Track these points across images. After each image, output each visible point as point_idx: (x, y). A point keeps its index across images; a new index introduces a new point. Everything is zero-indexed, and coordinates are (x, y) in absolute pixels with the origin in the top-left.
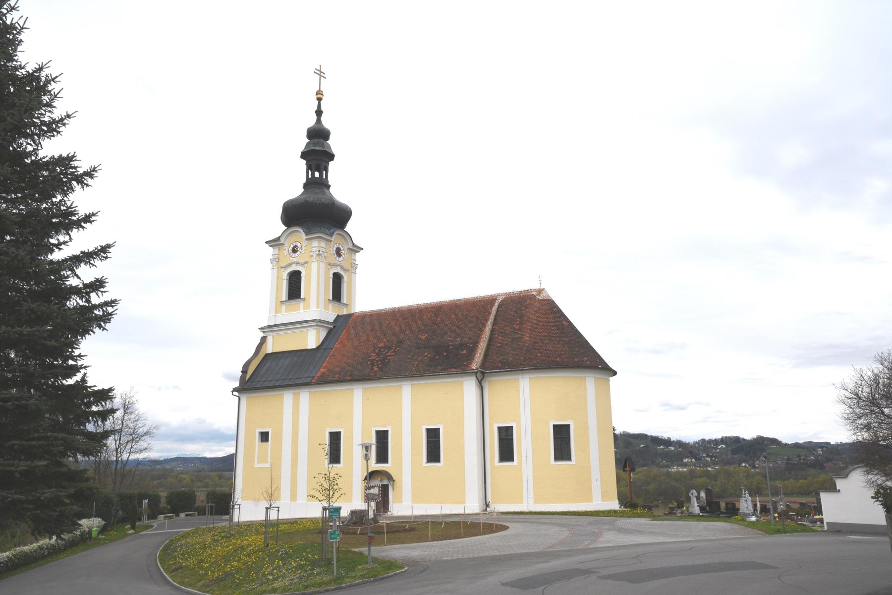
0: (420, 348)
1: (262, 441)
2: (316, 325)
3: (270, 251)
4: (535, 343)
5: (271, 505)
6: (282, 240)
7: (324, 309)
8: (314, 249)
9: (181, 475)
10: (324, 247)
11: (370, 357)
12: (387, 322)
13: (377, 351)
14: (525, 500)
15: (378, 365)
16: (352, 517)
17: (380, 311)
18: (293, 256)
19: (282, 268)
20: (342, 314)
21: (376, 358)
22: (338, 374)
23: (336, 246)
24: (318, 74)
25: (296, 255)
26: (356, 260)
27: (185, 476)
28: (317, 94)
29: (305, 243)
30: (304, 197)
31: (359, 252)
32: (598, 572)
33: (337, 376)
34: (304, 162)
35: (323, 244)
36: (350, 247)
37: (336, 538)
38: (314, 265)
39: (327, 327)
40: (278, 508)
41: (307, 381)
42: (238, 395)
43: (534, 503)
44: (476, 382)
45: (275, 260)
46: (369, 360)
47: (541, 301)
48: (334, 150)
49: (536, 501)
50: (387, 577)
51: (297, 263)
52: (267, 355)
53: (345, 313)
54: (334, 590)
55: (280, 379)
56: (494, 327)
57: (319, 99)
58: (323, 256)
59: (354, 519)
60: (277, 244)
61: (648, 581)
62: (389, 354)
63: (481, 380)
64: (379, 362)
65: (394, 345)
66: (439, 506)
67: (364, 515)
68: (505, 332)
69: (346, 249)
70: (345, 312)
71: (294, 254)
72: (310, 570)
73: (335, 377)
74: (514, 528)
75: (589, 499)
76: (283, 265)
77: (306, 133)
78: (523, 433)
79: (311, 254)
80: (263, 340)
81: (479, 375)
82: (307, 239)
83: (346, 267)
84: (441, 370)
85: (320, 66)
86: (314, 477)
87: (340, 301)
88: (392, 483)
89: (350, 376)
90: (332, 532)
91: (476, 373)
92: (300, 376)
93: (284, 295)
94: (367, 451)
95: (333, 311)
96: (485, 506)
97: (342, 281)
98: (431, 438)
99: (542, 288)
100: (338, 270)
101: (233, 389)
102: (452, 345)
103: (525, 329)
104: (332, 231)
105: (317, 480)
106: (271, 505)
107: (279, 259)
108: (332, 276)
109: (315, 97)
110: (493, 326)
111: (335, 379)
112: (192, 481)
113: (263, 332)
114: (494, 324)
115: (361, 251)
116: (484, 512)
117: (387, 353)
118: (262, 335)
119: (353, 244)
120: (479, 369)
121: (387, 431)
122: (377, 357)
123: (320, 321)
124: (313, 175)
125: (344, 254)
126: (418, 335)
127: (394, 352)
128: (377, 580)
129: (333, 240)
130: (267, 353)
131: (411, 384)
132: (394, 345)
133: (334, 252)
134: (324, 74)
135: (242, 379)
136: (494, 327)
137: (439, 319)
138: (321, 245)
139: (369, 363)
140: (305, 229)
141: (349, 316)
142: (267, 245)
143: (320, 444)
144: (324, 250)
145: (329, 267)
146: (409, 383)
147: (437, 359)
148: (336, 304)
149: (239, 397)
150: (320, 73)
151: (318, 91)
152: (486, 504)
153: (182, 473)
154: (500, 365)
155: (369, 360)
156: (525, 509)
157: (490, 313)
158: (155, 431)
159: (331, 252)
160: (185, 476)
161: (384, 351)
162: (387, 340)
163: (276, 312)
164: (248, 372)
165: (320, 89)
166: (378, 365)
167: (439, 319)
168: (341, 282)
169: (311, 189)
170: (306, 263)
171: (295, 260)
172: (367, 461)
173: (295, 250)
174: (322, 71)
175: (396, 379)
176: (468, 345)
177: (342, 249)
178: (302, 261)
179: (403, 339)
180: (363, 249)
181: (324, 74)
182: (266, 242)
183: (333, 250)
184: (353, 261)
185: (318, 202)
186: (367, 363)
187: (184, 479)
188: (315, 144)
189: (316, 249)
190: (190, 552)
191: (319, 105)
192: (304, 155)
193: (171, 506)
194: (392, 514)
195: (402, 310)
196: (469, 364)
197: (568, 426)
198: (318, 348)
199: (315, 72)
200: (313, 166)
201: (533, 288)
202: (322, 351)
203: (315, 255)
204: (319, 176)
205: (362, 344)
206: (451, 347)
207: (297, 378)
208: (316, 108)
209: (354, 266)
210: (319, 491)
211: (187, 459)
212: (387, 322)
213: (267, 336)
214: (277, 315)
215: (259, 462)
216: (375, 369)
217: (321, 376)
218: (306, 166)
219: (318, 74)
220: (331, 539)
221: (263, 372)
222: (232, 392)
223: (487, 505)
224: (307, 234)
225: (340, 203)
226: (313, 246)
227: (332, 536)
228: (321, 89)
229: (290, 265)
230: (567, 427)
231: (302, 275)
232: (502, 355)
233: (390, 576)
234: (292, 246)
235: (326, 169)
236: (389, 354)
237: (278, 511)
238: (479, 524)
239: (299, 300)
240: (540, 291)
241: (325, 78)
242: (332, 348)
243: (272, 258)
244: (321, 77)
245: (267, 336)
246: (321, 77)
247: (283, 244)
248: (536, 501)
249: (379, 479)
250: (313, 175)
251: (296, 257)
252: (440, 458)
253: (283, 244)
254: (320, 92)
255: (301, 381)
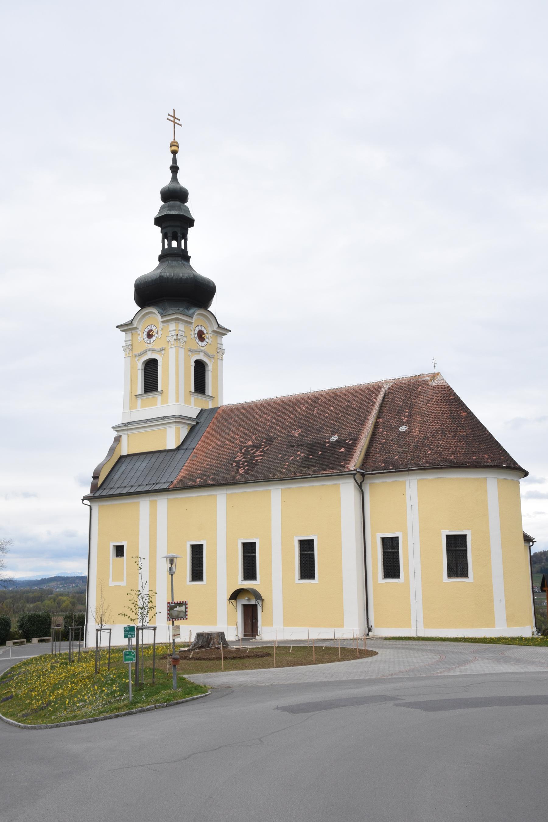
0: (293, 446)
1: (117, 556)
2: (176, 422)
3: (122, 336)
4: (425, 438)
5: (102, 627)
6: (135, 324)
7: (185, 403)
8: (171, 334)
9: (60, 597)
10: (183, 330)
11: (235, 458)
12: (257, 416)
13: (243, 451)
14: (413, 623)
15: (244, 466)
16: (198, 640)
17: (249, 403)
18: (149, 343)
19: (136, 356)
20: (208, 408)
21: (242, 459)
22: (199, 478)
23: (197, 329)
24: (171, 121)
25: (152, 340)
26: (222, 345)
27: (65, 598)
28: (171, 147)
29: (161, 326)
30: (153, 272)
31: (227, 334)
32: (403, 699)
33: (198, 480)
34: (159, 229)
35: (182, 327)
36: (215, 329)
37: (132, 660)
38: (172, 352)
39: (189, 424)
40: (110, 630)
41: (165, 486)
42: (89, 504)
43: (424, 628)
44: (354, 485)
45: (129, 347)
46: (235, 461)
47: (434, 388)
48: (194, 214)
49: (427, 625)
50: (183, 702)
51: (153, 350)
52: (121, 457)
53: (210, 407)
54: (124, 715)
55: (136, 484)
56: (378, 420)
57: (174, 153)
58: (181, 340)
59: (200, 643)
60: (130, 329)
61: (450, 710)
62: (257, 453)
63: (361, 483)
64: (245, 464)
65: (263, 444)
66: (332, 629)
67: (211, 638)
68: (391, 426)
69: (210, 331)
70: (210, 405)
71: (149, 340)
72: (120, 696)
73: (196, 482)
74: (384, 654)
75: (491, 624)
76: (138, 352)
77: (159, 196)
78: (410, 543)
79: (169, 338)
80: (117, 440)
81: (359, 478)
82: (163, 322)
83: (211, 354)
84: (314, 471)
85: (174, 110)
86: (127, 594)
87: (205, 393)
88: (260, 603)
89: (213, 480)
90: (128, 653)
91: (355, 474)
92: (157, 482)
93: (139, 387)
94: (172, 564)
95: (195, 405)
96: (367, 630)
97: (206, 369)
98: (304, 551)
99: (437, 372)
100: (201, 357)
101: (84, 497)
102: (328, 442)
103: (414, 422)
104: (191, 311)
105: (130, 597)
106: (102, 627)
107: (132, 346)
108: (193, 364)
109: (169, 150)
110: (377, 419)
111: (196, 484)
112: (73, 604)
113: (116, 431)
114: (378, 417)
115: (229, 334)
116: (368, 637)
117: (255, 452)
118: (115, 434)
119: (218, 325)
120: (358, 470)
121: (255, 543)
122: (244, 458)
123: (181, 417)
124: (170, 244)
125: (208, 338)
126: (291, 431)
127: (263, 451)
128: (170, 705)
129: (193, 321)
130: (122, 455)
131: (281, 489)
132: (263, 444)
133: (196, 336)
134: (179, 120)
135: (94, 488)
136: (378, 420)
137: (315, 412)
138: (179, 329)
139: (234, 464)
140: (160, 310)
141: (213, 411)
142: (118, 330)
143: (132, 557)
144: (183, 334)
145: (190, 353)
146: (279, 487)
147: (311, 458)
148: (199, 397)
149: (90, 506)
150: (174, 120)
151: (172, 143)
152: (368, 627)
153: (62, 595)
154: (383, 465)
155: (235, 461)
156: (413, 635)
157: (374, 403)
158: (8, 546)
159: (192, 336)
160: (65, 598)
161: (252, 450)
162: (256, 438)
163: (131, 407)
164: (100, 477)
165: (174, 140)
166: (244, 466)
167: (315, 412)
168: (205, 370)
169: (167, 262)
170: (163, 349)
171: (150, 347)
172: (172, 575)
173: (150, 335)
174: (176, 117)
175: (273, 482)
176: (347, 441)
177: (205, 332)
178: (158, 348)
179: (273, 435)
180: (230, 331)
181: (179, 120)
182: (117, 327)
183: (194, 334)
184: (218, 345)
185: (174, 278)
186: (232, 464)
187: (64, 601)
188: (170, 208)
189: (174, 333)
190: (24, 680)
191: (175, 160)
192: (159, 221)
193: (23, 631)
194: (261, 639)
195: (274, 402)
196: (347, 464)
197: (464, 537)
198: (178, 448)
199: (168, 119)
200: (169, 234)
201: (426, 372)
202: (182, 451)
203: (172, 340)
204: (178, 245)
205: (227, 442)
206: (327, 445)
207: (154, 484)
208: (170, 164)
209: (220, 351)
210: (131, 609)
211: (68, 578)
212: (257, 416)
213: (121, 436)
214: (131, 411)
215: (113, 580)
216: (241, 471)
217: (181, 480)
218: (161, 234)
219: (171, 121)
220: (126, 660)
221: (116, 477)
222: (83, 500)
223: (370, 630)
224: (162, 316)
225: (203, 277)
226: (170, 329)
227: (128, 657)
228: (176, 140)
229: (145, 352)
230: (463, 538)
231: (159, 364)
232: (386, 453)
233: (186, 701)
234: (147, 330)
235: (185, 237)
236: (257, 453)
237: (110, 633)
238: (336, 649)
239: (155, 393)
240: (434, 376)
241: (181, 125)
242: (194, 449)
243: (124, 345)
244: (175, 124)
245: (121, 436)
246: (175, 124)
247: (136, 328)
248: (427, 625)
249: (246, 598)
250: (170, 244)
251: (151, 343)
252: (314, 574)
253: (136, 328)
254: (175, 144)
255: (157, 487)
